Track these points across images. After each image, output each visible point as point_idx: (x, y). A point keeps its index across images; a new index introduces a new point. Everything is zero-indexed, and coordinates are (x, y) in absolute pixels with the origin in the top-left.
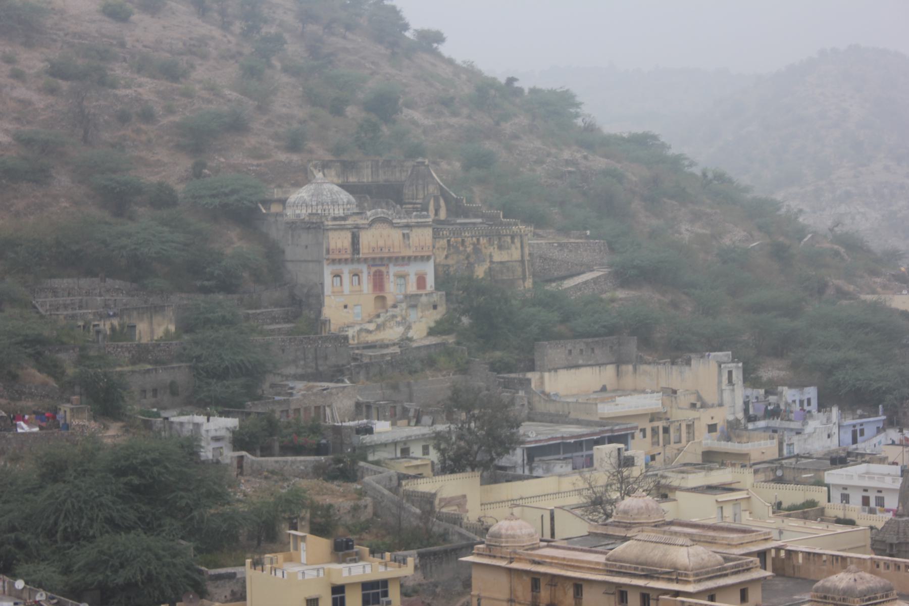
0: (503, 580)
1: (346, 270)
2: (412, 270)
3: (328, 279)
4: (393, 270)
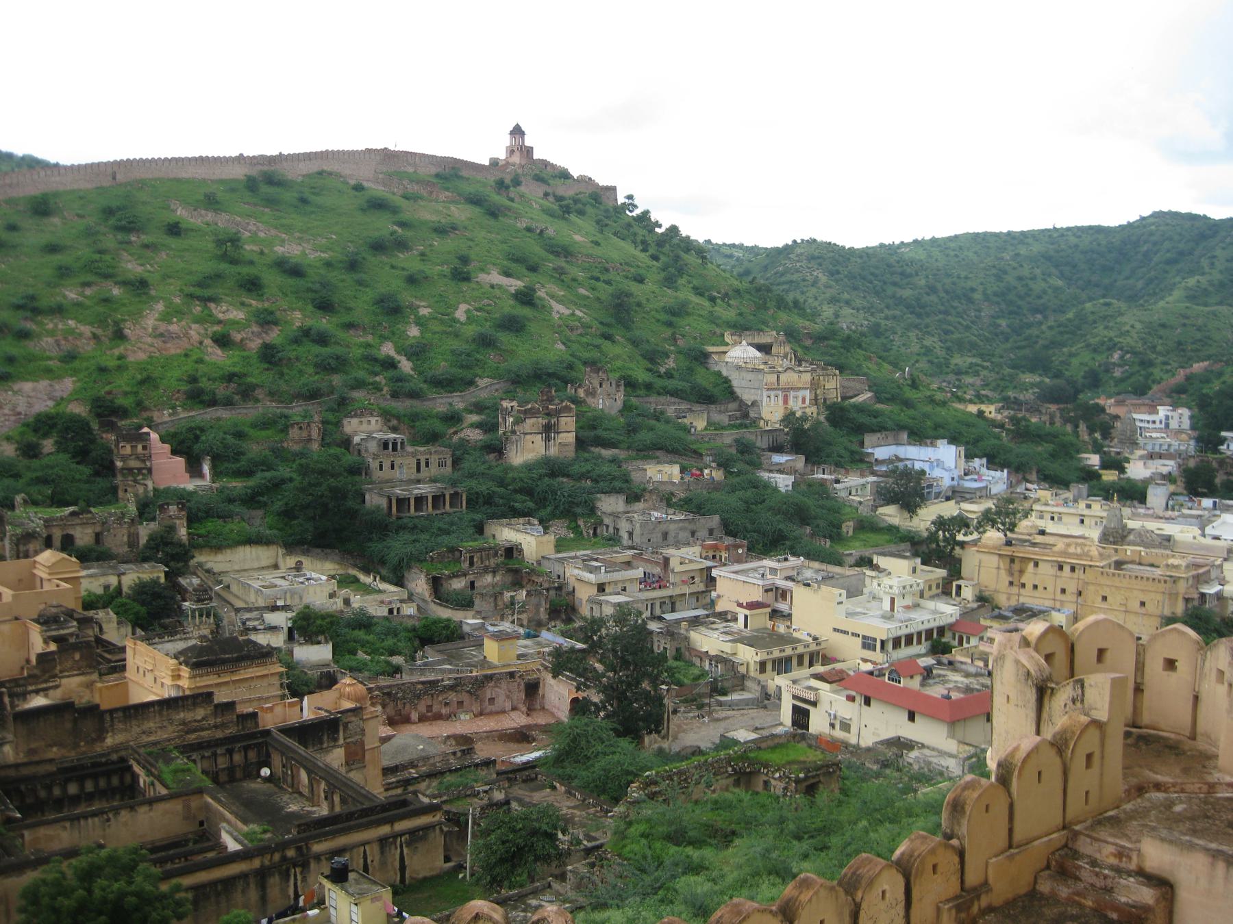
0: (996, 558)
1: (772, 393)
2: (801, 394)
3: (765, 398)
4: (792, 394)
